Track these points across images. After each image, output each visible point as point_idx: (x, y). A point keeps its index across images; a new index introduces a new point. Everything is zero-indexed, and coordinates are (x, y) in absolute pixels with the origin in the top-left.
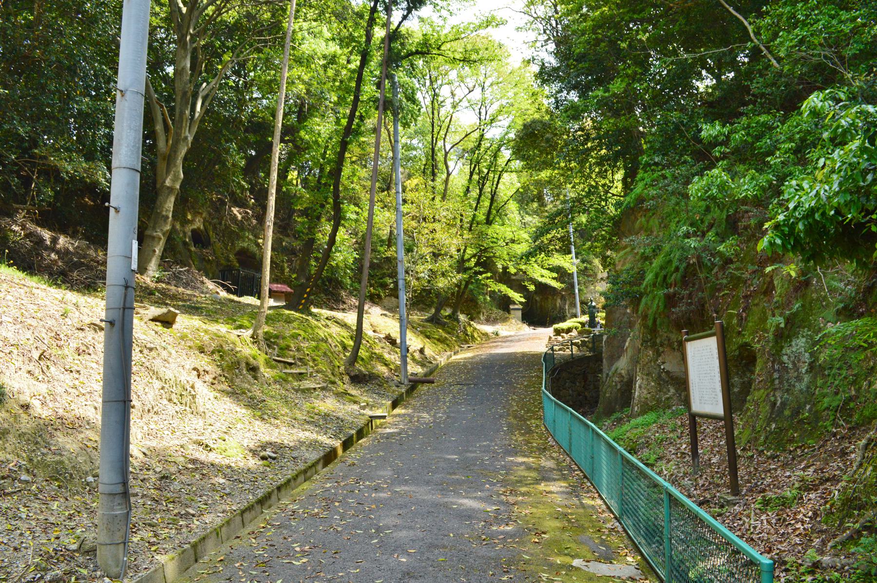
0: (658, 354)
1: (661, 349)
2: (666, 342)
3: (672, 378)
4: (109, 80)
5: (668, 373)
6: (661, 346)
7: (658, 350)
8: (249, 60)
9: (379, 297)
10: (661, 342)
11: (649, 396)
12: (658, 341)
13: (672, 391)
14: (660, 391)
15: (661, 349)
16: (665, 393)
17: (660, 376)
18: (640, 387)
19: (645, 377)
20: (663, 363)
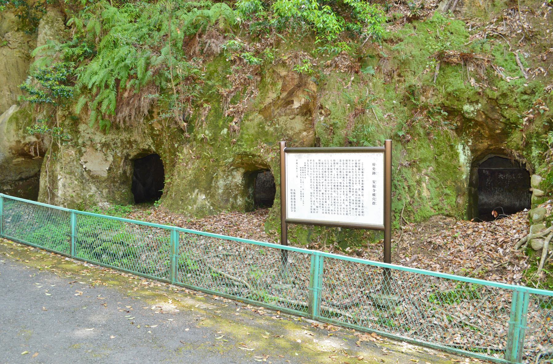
0: (81, 153)
1: (83, 149)
2: (89, 143)
3: (93, 177)
4: (6, 110)
5: (89, 172)
6: (84, 146)
7: (80, 151)
8: (420, 60)
9: (338, 249)
10: (84, 143)
11: (74, 194)
12: (80, 141)
13: (94, 188)
14: (83, 189)
15: (83, 149)
16: (89, 192)
17: (82, 175)
18: (64, 186)
19: (68, 176)
20: (85, 162)
